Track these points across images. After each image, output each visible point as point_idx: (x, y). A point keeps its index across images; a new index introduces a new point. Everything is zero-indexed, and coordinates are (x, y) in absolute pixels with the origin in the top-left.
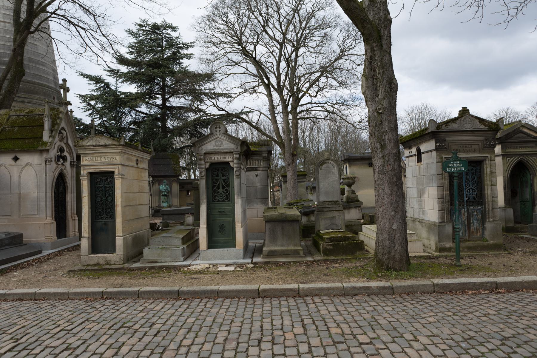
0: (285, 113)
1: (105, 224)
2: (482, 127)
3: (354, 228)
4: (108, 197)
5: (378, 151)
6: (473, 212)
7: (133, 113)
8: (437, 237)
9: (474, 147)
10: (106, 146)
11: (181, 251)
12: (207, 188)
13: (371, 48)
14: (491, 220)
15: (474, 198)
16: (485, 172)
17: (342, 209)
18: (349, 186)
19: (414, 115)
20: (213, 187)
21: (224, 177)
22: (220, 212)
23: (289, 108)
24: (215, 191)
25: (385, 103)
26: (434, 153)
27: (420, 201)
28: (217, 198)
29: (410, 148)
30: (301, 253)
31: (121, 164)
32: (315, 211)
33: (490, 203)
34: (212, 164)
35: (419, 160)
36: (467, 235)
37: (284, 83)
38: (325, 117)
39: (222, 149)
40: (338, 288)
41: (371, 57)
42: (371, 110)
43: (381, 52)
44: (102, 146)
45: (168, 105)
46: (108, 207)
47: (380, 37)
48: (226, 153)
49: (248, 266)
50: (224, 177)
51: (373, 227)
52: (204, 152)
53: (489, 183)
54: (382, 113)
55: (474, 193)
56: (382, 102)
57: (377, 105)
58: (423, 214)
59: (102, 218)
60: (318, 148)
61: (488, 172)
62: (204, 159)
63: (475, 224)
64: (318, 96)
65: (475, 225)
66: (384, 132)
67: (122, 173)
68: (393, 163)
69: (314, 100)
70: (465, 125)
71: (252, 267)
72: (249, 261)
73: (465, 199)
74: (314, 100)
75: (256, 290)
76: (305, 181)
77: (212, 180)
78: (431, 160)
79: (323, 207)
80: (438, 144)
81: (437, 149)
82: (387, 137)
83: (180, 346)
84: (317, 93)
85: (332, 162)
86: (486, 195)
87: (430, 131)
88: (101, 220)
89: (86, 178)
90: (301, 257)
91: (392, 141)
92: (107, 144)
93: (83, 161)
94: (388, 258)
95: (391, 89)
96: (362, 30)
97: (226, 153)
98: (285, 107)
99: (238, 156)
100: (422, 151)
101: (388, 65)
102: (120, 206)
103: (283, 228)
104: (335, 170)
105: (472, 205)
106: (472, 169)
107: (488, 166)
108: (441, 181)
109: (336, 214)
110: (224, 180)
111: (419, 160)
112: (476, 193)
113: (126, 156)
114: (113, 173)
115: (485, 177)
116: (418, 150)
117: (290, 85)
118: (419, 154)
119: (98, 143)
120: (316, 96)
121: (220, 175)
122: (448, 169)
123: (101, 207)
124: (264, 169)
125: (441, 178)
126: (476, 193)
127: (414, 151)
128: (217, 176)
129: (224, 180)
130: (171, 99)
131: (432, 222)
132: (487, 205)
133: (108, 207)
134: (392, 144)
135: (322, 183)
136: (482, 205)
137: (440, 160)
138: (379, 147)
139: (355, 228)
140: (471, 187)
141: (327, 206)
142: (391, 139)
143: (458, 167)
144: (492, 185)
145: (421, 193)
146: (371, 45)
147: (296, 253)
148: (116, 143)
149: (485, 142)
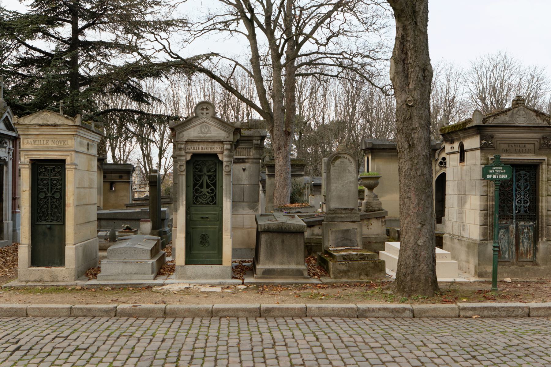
0: (277, 67)
1: (50, 229)
2: (539, 121)
3: (375, 245)
4: (55, 192)
5: (405, 152)
6: (523, 229)
7: (23, 49)
8: (477, 259)
9: (528, 146)
10: (55, 126)
11: (150, 266)
12: (187, 186)
13: (403, 26)
14: (545, 239)
15: (526, 212)
16: (541, 179)
17: (359, 220)
18: (371, 188)
19: (484, 69)
20: (195, 185)
21: (210, 173)
22: (202, 218)
23: (283, 61)
24: (196, 191)
25: (417, 94)
26: (479, 152)
27: (461, 213)
28: (199, 199)
29: (452, 142)
30: (306, 274)
31: (75, 151)
32: (323, 221)
33: (544, 218)
34: (195, 156)
35: (462, 159)
36: (515, 257)
37: (277, 18)
38: (339, 73)
39: (210, 137)
40: (352, 308)
41: (403, 37)
42: (399, 101)
43: (414, 31)
44: (52, 125)
45: (81, 38)
46: (54, 206)
47: (414, 12)
48: (214, 142)
49: (239, 287)
50: (210, 173)
51: (397, 245)
52: (186, 139)
53: (544, 193)
54: (412, 106)
55: (526, 205)
56: (413, 93)
57: (407, 96)
58: (464, 229)
59: (45, 220)
60: (323, 118)
61: (544, 179)
62: (185, 149)
63: (526, 244)
64: (330, 44)
65: (525, 245)
66: (413, 129)
67: (76, 162)
68: (422, 167)
69: (322, 49)
70: (518, 119)
71: (245, 289)
72: (240, 281)
73: (515, 212)
74: (322, 49)
75: (257, 309)
76: (302, 176)
77: (194, 176)
78: (474, 159)
79: (333, 216)
80: (483, 142)
81: (482, 148)
82: (416, 135)
83: (194, 349)
84: (328, 39)
85: (348, 157)
86: (540, 208)
87: (474, 124)
88: (44, 223)
89: (27, 166)
90: (306, 278)
91: (423, 140)
92: (58, 123)
93: (23, 143)
94: (411, 279)
95: (424, 77)
96: (393, 4)
97: (214, 142)
98: (277, 56)
99: (229, 147)
100: (465, 148)
101: (422, 48)
102: (72, 205)
103: (283, 242)
104: (352, 168)
105: (523, 220)
106: (525, 175)
107: (544, 171)
108: (485, 189)
109: (350, 226)
110: (209, 177)
111: (462, 159)
112: (528, 204)
113: (79, 139)
114: (64, 161)
115: (540, 186)
116: (461, 146)
117: (285, 20)
118: (462, 152)
119: (45, 122)
120: (327, 43)
121: (205, 170)
122: (489, 176)
123: (45, 206)
124: (255, 161)
125: (485, 184)
126: (528, 204)
127: (456, 146)
128: (201, 171)
129: (209, 177)
130: (86, 31)
131: (473, 240)
132: (540, 220)
133: (54, 206)
134: (423, 144)
135: (335, 185)
136: (535, 220)
137: (485, 162)
138: (407, 146)
139: (374, 246)
140: (522, 197)
141: (340, 215)
142: (421, 138)
143: (500, 173)
144: (548, 196)
145: (462, 202)
146: (403, 23)
147: (299, 274)
148: (71, 123)
149: (542, 142)
